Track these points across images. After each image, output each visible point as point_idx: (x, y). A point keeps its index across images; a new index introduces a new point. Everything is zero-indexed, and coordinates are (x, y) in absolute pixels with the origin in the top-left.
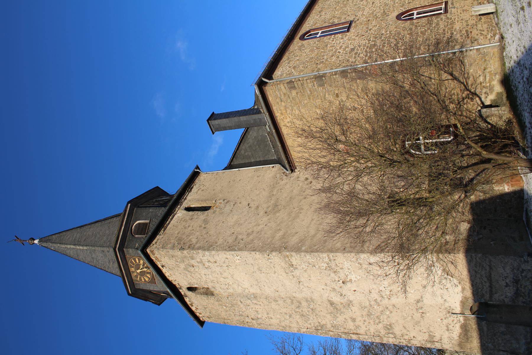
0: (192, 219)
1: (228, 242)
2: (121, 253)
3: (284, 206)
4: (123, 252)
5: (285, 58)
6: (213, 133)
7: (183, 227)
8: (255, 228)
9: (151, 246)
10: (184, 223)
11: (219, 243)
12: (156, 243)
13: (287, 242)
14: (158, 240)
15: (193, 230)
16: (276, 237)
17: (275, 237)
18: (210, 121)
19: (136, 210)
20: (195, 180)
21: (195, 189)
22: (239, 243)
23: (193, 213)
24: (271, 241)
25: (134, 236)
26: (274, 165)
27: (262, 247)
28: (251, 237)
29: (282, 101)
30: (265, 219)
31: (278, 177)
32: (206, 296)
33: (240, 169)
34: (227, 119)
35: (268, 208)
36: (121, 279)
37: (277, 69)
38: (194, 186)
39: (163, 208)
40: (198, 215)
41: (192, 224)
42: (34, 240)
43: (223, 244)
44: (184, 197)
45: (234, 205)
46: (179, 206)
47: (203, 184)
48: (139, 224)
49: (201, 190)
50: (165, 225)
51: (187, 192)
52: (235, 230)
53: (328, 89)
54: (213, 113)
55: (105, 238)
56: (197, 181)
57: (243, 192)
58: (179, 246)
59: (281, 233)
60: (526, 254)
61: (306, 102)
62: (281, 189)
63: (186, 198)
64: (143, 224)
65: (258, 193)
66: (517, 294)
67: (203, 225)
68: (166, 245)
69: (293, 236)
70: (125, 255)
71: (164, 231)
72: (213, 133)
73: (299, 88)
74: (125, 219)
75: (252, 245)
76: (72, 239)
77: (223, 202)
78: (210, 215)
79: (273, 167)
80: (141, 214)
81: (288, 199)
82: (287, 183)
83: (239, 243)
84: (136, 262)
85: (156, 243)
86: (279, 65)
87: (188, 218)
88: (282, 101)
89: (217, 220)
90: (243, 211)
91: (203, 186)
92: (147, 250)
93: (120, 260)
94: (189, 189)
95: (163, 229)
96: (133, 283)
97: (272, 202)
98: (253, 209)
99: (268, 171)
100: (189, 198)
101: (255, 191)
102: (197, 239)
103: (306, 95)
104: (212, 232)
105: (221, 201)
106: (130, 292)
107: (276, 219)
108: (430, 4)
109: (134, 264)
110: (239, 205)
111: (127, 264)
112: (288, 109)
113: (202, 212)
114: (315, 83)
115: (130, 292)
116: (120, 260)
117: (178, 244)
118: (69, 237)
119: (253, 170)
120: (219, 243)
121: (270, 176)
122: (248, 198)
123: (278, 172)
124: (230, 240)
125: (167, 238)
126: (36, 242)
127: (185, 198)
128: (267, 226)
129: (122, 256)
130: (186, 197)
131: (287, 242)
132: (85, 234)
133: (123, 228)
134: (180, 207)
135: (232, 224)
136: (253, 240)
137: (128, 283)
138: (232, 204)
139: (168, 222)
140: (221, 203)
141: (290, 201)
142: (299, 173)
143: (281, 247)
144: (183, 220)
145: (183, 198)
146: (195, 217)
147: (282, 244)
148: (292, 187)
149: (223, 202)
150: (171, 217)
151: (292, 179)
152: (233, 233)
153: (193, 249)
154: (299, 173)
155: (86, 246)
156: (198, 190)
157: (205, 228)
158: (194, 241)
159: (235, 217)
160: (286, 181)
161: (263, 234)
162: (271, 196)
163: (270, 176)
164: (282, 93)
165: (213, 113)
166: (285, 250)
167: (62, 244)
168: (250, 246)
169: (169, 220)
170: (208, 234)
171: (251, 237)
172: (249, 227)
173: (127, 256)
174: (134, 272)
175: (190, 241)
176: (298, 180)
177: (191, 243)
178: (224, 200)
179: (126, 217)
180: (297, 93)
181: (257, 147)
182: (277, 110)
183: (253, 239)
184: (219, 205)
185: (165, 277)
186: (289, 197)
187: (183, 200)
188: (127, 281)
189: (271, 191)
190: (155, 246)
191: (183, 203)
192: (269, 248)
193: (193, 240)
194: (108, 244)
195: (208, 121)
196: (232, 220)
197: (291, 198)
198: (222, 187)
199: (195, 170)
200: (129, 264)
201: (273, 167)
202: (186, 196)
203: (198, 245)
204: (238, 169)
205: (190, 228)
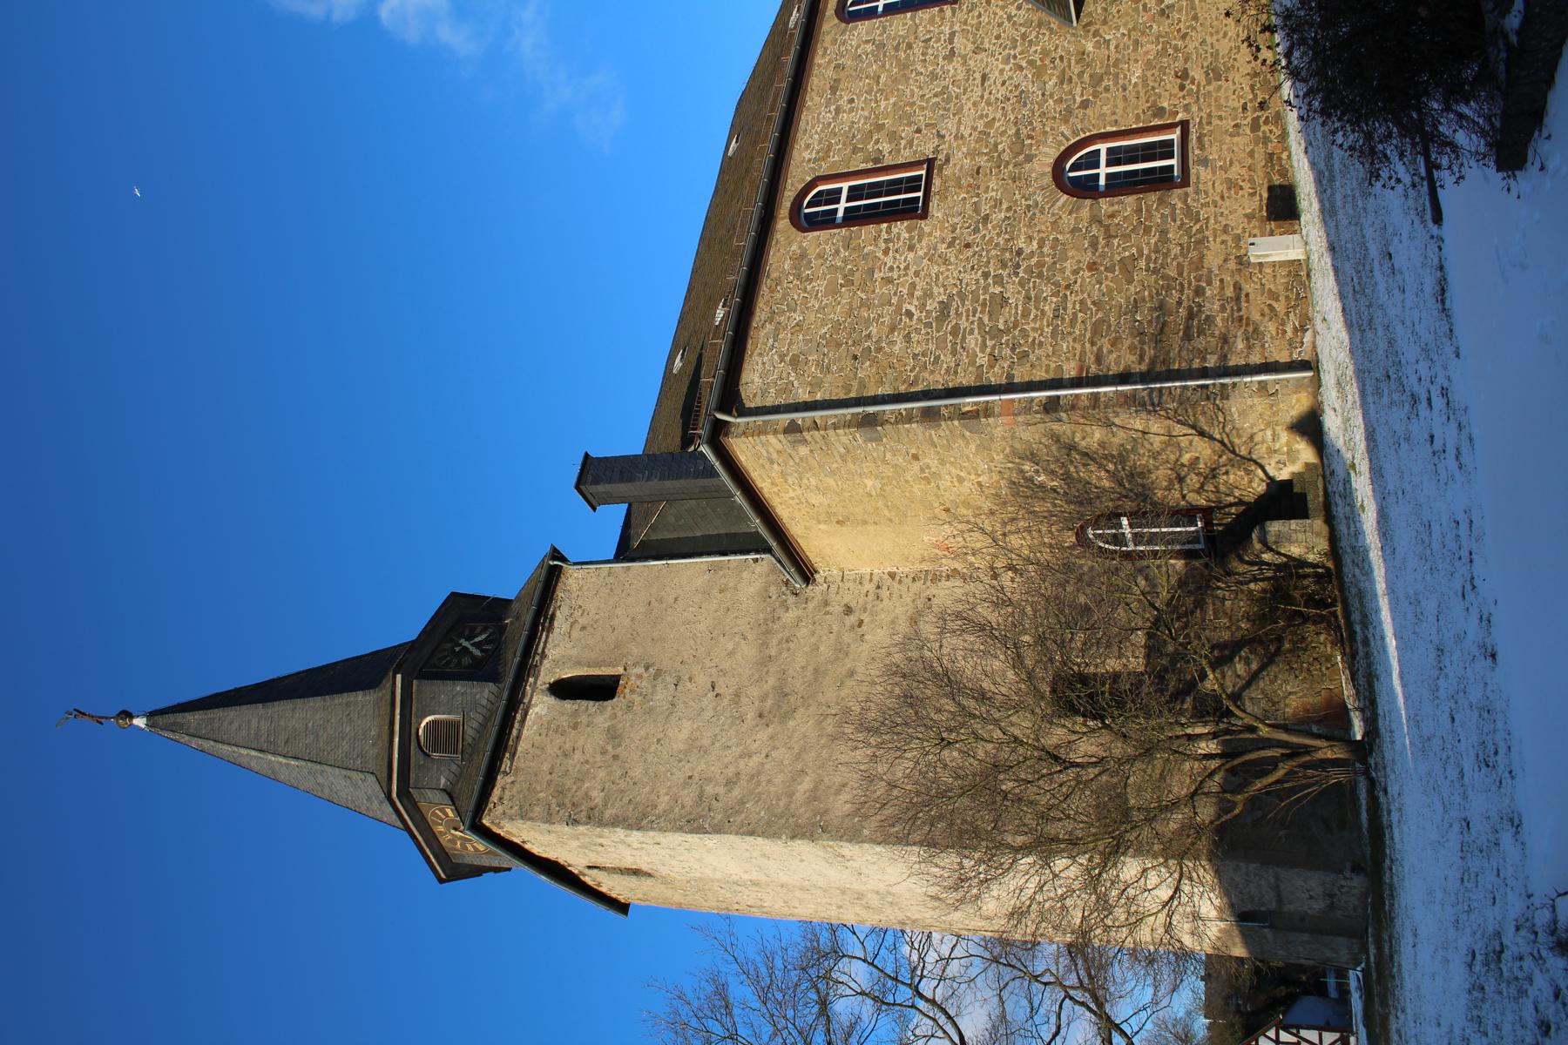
0: (575, 726)
1: (683, 807)
2: (405, 800)
3: (802, 697)
4: (410, 796)
5: (761, 313)
6: (594, 509)
7: (559, 753)
8: (742, 763)
9: (490, 810)
10: (559, 740)
11: (661, 808)
12: (501, 799)
13: (826, 811)
14: (503, 789)
15: (587, 762)
16: (798, 794)
17: (794, 794)
18: (582, 487)
19: (418, 686)
20: (554, 591)
21: (561, 625)
22: (709, 810)
23: (576, 707)
24: (787, 807)
25: (429, 756)
26: (758, 556)
27: (769, 824)
28: (736, 793)
29: (772, 462)
30: (763, 735)
31: (774, 597)
32: (634, 877)
33: (669, 562)
34: (629, 485)
35: (763, 699)
36: (405, 834)
37: (745, 366)
38: (558, 612)
39: (491, 684)
40: (589, 712)
41: (580, 743)
42: (130, 716)
43: (671, 810)
44: (537, 649)
45: (676, 685)
46: (531, 680)
47: (580, 607)
48: (434, 722)
49: (577, 627)
50: (511, 743)
51: (543, 630)
52: (692, 769)
53: (891, 447)
54: (587, 455)
55: (345, 744)
56: (560, 594)
57: (692, 642)
58: (564, 813)
59: (806, 785)
60: (1348, 865)
61: (835, 465)
62: (787, 641)
63: (543, 651)
64: (448, 723)
65: (730, 646)
66: (1331, 907)
67: (609, 748)
68: (527, 807)
69: (838, 792)
70: (415, 802)
71: (512, 759)
72: (594, 509)
73: (816, 442)
74: (398, 717)
75: (743, 815)
76: (249, 734)
77: (645, 675)
78: (619, 714)
79: (756, 561)
80: (434, 698)
81: (809, 672)
82: (799, 619)
83: (709, 810)
84: (447, 816)
85: (501, 799)
86: (750, 341)
87: (564, 721)
88: (772, 462)
89: (642, 733)
90: (704, 706)
91: (580, 611)
92: (484, 821)
93: (406, 817)
94: (545, 621)
95: (507, 755)
96: (447, 854)
97: (772, 681)
98: (726, 702)
99: (745, 574)
100: (552, 653)
101: (722, 639)
102: (603, 790)
103: (836, 454)
104: (637, 773)
105: (640, 670)
106: (443, 876)
107: (790, 737)
108: (1141, 125)
109: (442, 820)
110: (688, 684)
111: (424, 818)
112: (789, 478)
113: (597, 704)
114: (858, 436)
115: (443, 876)
116: (406, 817)
117: (559, 805)
118: (236, 724)
119: (705, 567)
120: (661, 808)
121: (752, 589)
122: (707, 661)
123: (771, 578)
124: (688, 797)
125: (525, 786)
126: (140, 722)
127: (540, 651)
128: (770, 758)
129: (410, 807)
130: (544, 648)
131: (826, 811)
132: (282, 723)
133: (397, 740)
134: (535, 683)
135: (682, 747)
136: (742, 802)
137: (435, 857)
138: (671, 680)
139: (515, 732)
140: (640, 677)
141: (816, 680)
142: (825, 585)
143: (813, 825)
144: (549, 728)
145: (536, 653)
146: (583, 719)
147: (815, 815)
148: (813, 633)
149: (645, 675)
150: (519, 717)
151: (811, 606)
152: (690, 777)
153: (601, 823)
154: (825, 585)
155: (296, 758)
156: (571, 626)
157: (616, 757)
158: (598, 797)
159: (687, 725)
160: (796, 614)
161: (764, 784)
162: (765, 661)
163: (752, 589)
164: (771, 450)
165: (587, 455)
166: (825, 836)
167: (223, 743)
168: (739, 818)
169: (516, 725)
170: (628, 779)
171: (736, 793)
172: (726, 760)
173: (422, 805)
174: (445, 834)
175: (587, 796)
176: (827, 613)
177: (592, 804)
178: (647, 668)
179: (398, 711)
180: (811, 451)
181: (709, 510)
182: (761, 477)
183: (741, 799)
184: (638, 683)
185: (532, 855)
186: (810, 668)
187: (537, 658)
188: (431, 856)
189: (762, 644)
190: (500, 808)
191: (539, 671)
192: (786, 828)
193: (594, 794)
194: (359, 762)
195: (577, 487)
196: (681, 732)
197: (816, 670)
198: (633, 619)
199: (551, 563)
200: (429, 817)
201: (756, 561)
202: (542, 645)
203: (609, 813)
204: (664, 562)
205: (578, 755)
